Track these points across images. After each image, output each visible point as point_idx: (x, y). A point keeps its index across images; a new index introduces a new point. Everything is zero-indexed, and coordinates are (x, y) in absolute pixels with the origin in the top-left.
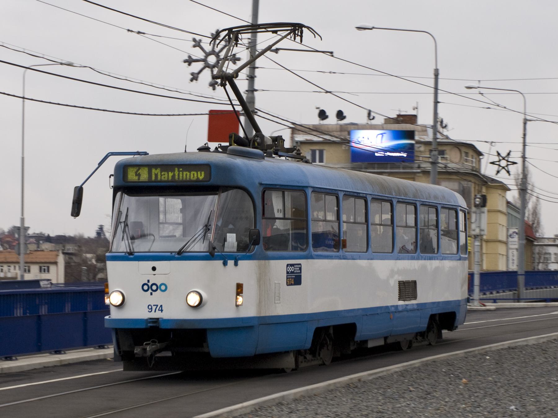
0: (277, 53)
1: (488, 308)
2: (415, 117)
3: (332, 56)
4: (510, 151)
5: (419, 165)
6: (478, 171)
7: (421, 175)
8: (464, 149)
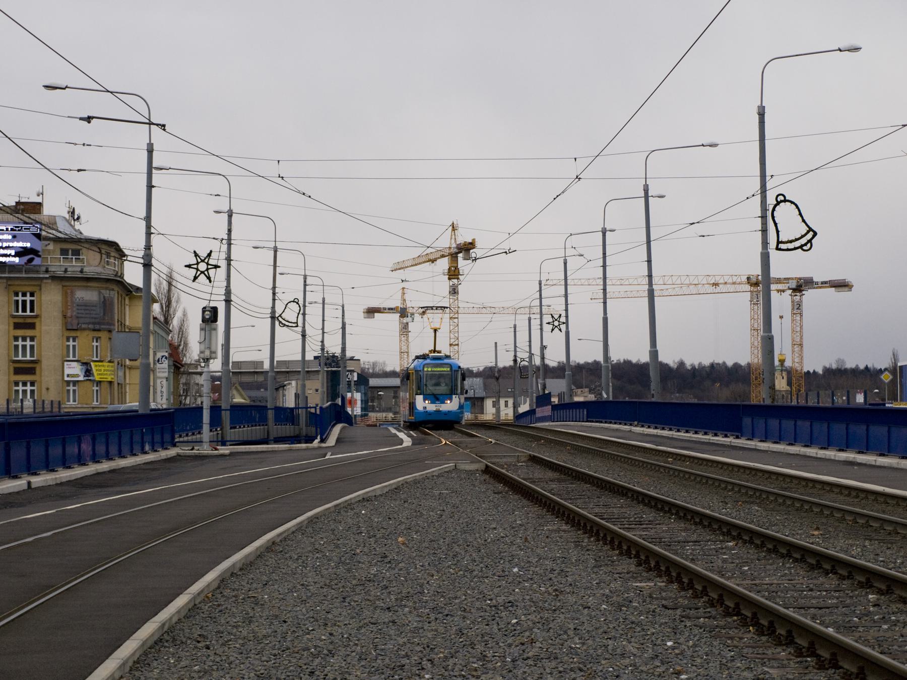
0: (89, 122)
1: (221, 452)
2: (40, 205)
3: (164, 130)
4: (211, 251)
5: (47, 269)
6: (122, 276)
7: (50, 281)
8: (105, 248)
